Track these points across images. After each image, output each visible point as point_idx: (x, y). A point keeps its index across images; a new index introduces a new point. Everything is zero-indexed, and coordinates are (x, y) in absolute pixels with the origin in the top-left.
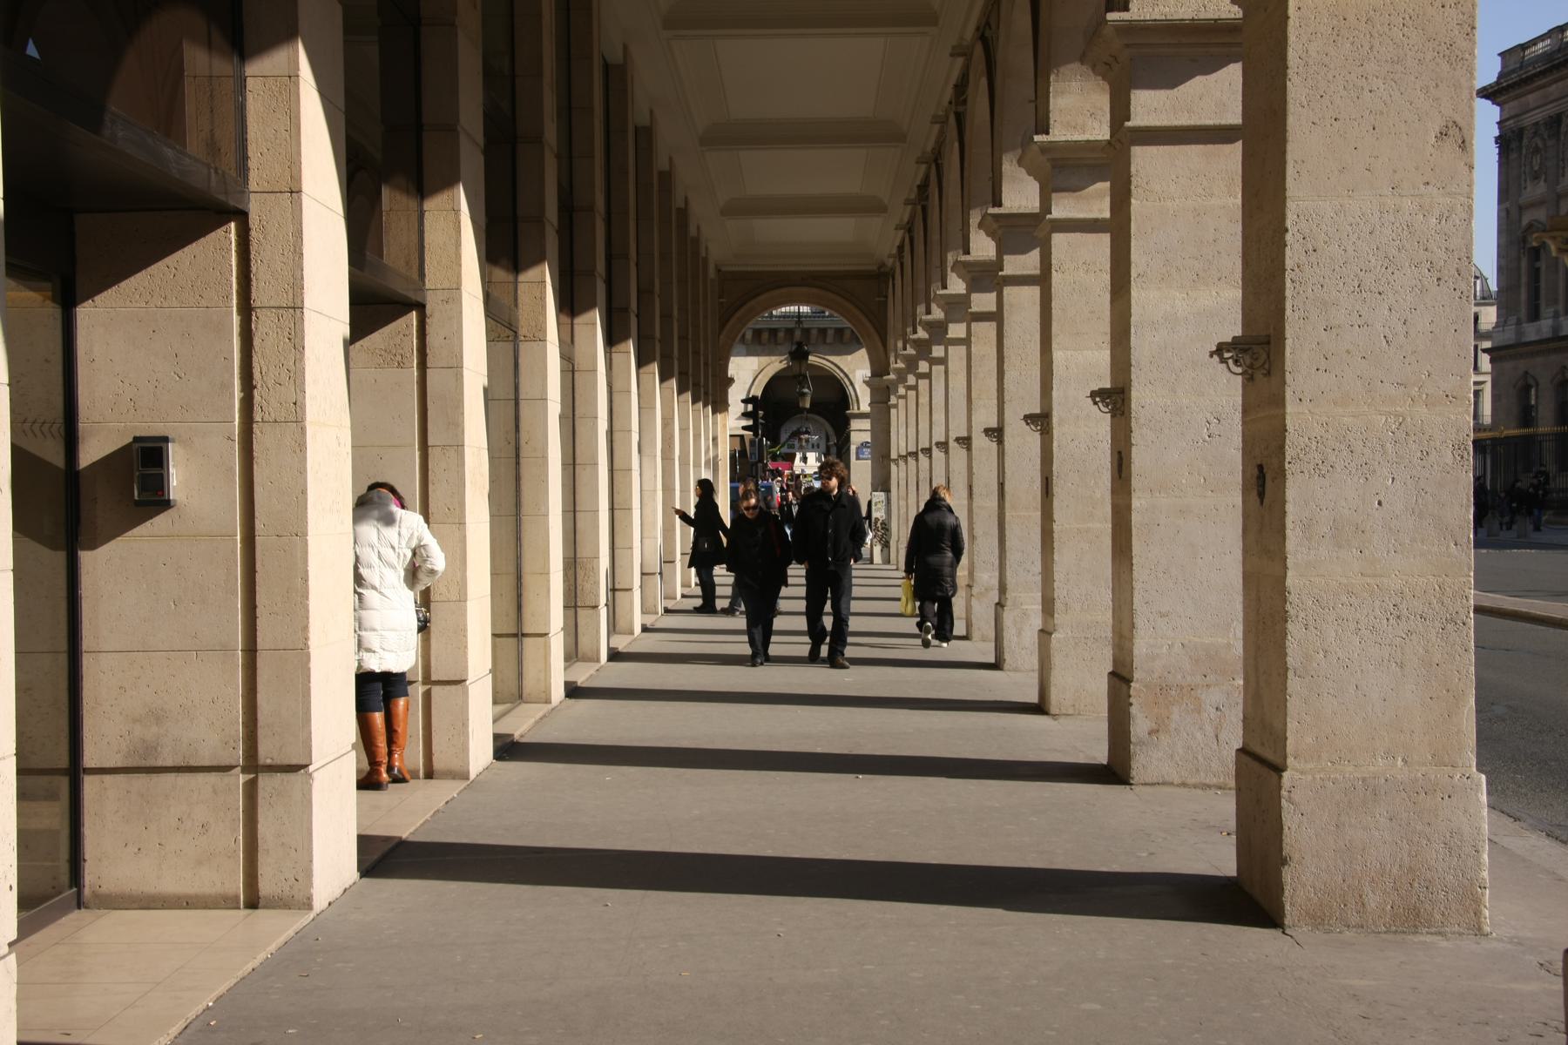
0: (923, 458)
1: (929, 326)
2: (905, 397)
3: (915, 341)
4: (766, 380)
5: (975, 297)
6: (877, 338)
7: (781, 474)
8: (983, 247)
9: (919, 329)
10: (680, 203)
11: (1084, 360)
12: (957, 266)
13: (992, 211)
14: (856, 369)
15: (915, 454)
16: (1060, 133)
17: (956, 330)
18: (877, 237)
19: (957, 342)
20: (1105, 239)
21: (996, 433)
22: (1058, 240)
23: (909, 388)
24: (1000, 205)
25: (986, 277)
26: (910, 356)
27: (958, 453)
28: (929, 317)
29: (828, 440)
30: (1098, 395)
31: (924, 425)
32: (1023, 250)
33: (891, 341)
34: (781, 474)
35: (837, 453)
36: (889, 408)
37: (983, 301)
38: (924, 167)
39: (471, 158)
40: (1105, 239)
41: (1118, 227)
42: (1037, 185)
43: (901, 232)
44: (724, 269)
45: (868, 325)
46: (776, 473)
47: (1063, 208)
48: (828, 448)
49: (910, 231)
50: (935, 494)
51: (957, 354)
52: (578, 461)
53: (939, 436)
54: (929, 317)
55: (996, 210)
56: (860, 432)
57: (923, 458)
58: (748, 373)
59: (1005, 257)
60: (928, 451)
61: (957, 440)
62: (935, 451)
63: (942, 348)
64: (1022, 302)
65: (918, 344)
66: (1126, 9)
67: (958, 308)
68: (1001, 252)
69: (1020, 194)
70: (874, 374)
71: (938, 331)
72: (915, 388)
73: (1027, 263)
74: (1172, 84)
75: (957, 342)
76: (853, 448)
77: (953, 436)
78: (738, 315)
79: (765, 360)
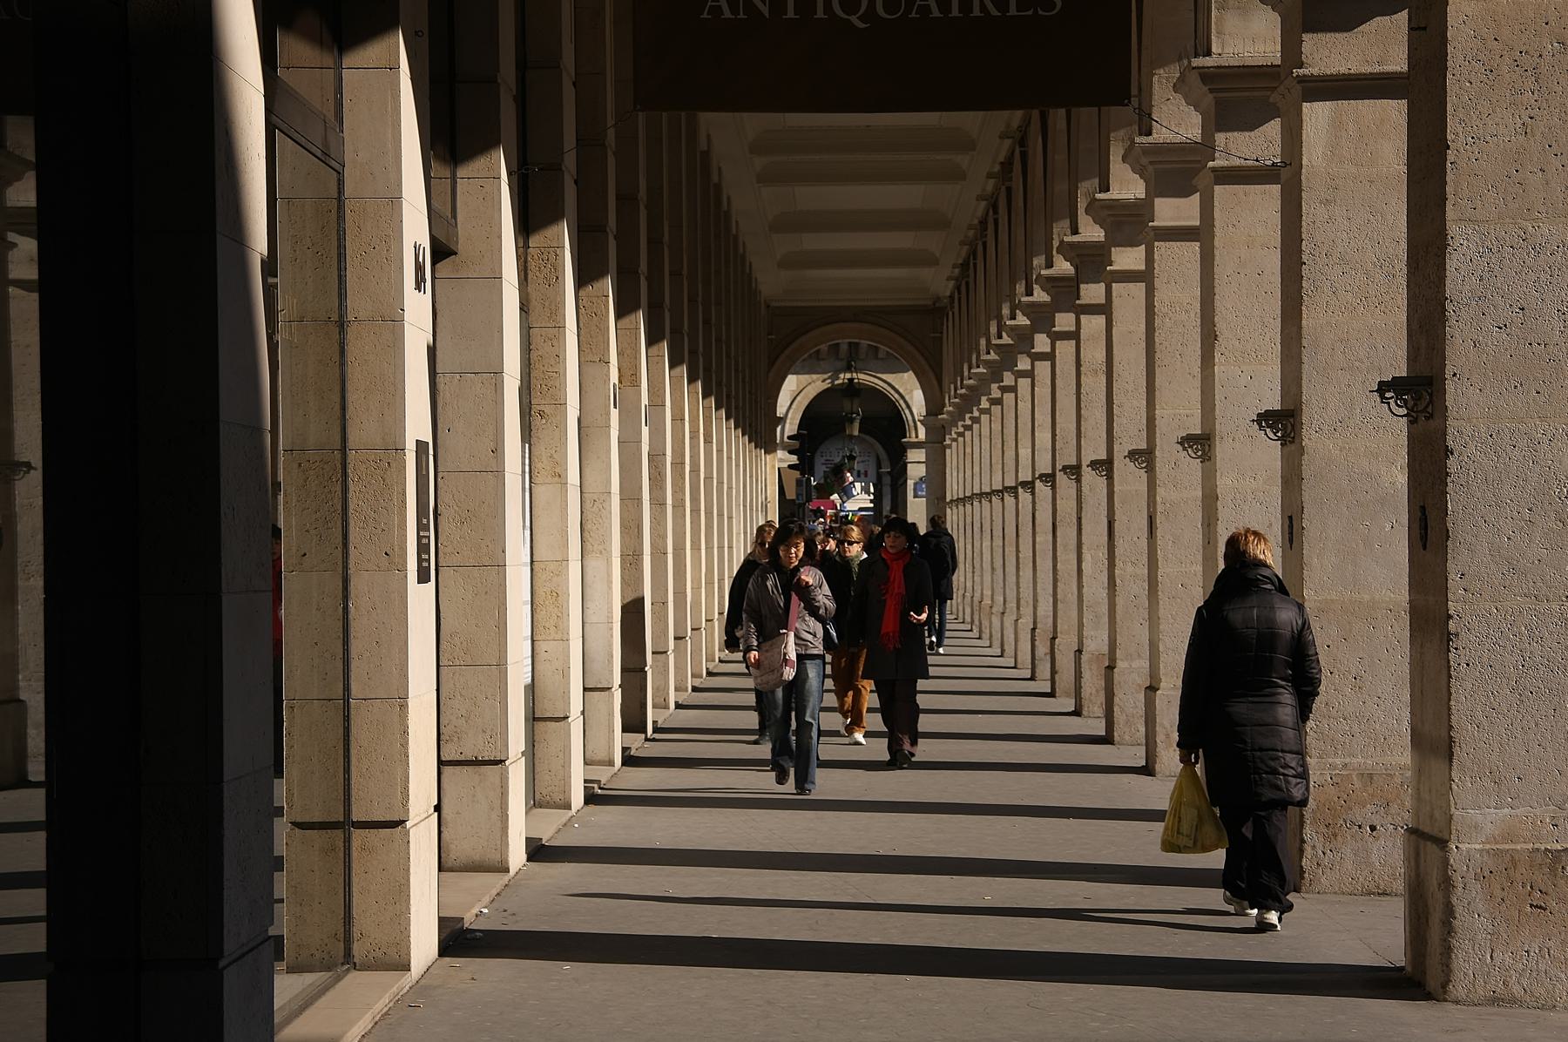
0: (1025, 497)
1: (1052, 283)
2: (987, 411)
3: (1013, 329)
4: (806, 403)
5: (1160, 203)
6: (932, 375)
7: (823, 516)
8: (1127, 186)
9: (1037, 289)
10: (703, 146)
11: (1363, 329)
12: (1094, 208)
13: (1196, 62)
14: (911, 393)
15: (1013, 490)
16: (1161, 135)
17: (1127, 258)
18: (939, 282)
19: (1128, 276)
20: (1394, 112)
21: (1283, 422)
22: (1317, 116)
23: (1021, 374)
24: (1209, 53)
25: (1129, 223)
26: (994, 361)
27: (1130, 477)
28: (1150, 139)
29: (879, 466)
30: (1267, 419)
31: (1025, 452)
32: (1250, 123)
33: (946, 380)
34: (823, 516)
35: (891, 485)
36: (945, 448)
37: (1173, 211)
38: (1008, 142)
39: (613, 264)
40: (1394, 112)
41: (1422, 87)
42: (1275, 19)
43: (1008, 142)
44: (774, 304)
45: (923, 362)
46: (819, 513)
47: (1328, 54)
48: (879, 477)
49: (1022, 142)
50: (1239, 576)
51: (1129, 298)
52: (351, 444)
53: (1044, 467)
54: (1076, 238)
55: (1144, 139)
56: (916, 466)
57: (1025, 497)
58: (795, 393)
59: (1158, 201)
60: (1029, 485)
61: (1064, 468)
62: (1088, 475)
63: (1072, 316)
64: (1250, 217)
65: (1032, 310)
66: (1209, 53)
67: (1129, 223)
68: (1208, 132)
69: (1127, 186)
70: (929, 413)
71: (1092, 262)
72: (1030, 374)
73: (1257, 144)
74: (1251, 127)
75: (1128, 276)
76: (910, 483)
77: (1120, 451)
78: (787, 352)
79: (805, 378)
